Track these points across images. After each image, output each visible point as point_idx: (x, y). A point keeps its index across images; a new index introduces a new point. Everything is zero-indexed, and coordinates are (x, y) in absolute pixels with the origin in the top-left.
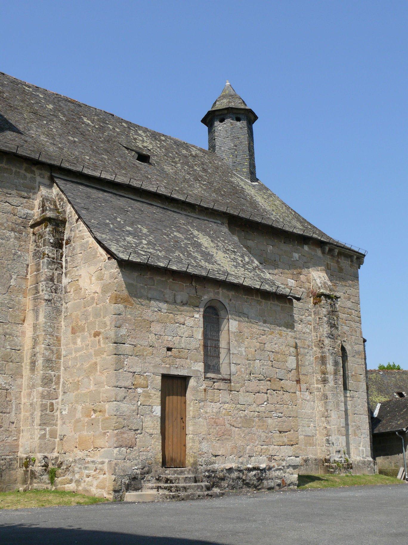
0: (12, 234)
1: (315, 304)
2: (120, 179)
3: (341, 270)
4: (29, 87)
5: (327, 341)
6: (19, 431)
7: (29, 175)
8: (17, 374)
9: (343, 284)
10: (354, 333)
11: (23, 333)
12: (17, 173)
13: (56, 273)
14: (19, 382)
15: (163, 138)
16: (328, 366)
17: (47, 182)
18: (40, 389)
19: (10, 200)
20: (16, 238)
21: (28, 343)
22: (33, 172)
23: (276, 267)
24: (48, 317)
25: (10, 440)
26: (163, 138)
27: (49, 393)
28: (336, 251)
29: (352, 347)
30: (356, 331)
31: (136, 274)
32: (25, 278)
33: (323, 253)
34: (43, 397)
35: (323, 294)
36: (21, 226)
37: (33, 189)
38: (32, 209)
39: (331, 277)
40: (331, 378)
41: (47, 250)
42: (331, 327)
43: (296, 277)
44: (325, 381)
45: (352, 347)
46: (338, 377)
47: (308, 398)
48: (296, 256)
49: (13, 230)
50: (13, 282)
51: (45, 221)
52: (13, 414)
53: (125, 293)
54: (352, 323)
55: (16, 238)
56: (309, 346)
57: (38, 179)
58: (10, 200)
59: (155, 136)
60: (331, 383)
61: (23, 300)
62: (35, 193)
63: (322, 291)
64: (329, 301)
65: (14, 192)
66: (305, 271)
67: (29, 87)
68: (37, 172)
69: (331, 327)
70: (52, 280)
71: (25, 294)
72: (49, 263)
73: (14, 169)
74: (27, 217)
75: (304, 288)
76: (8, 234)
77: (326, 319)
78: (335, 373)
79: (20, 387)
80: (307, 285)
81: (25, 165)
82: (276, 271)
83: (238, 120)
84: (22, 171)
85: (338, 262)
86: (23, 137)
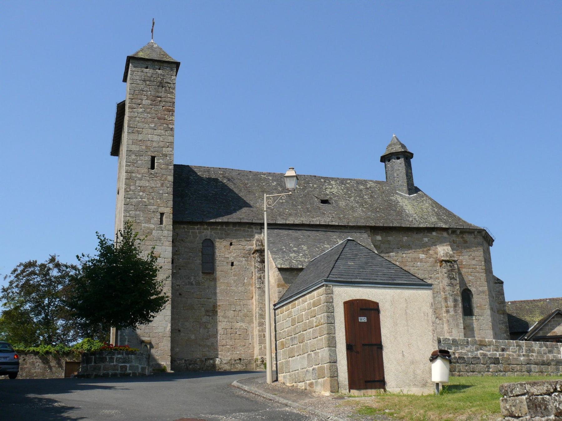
0: (244, 259)
1: (440, 266)
2: (297, 222)
3: (466, 242)
4: (264, 174)
5: (447, 288)
6: (254, 348)
7: (250, 230)
8: (251, 322)
9: (468, 250)
10: (479, 280)
11: (253, 303)
12: (244, 231)
13: (262, 275)
14: (252, 325)
15: (349, 181)
16: (449, 303)
17: (259, 231)
18: (258, 328)
19: (241, 243)
20: (245, 260)
21: (254, 309)
22: (252, 228)
23: (411, 249)
24: (259, 295)
25: (250, 351)
26: (349, 181)
27: (262, 329)
28: (458, 232)
29: (477, 289)
30: (480, 279)
31: (288, 273)
32: (252, 278)
33: (448, 234)
34: (259, 331)
35: (443, 261)
36: (247, 255)
37: (252, 236)
38: (253, 245)
39: (453, 249)
40: (451, 310)
41: (257, 265)
42: (451, 279)
43: (426, 253)
44: (448, 312)
45: (477, 289)
46: (457, 308)
47: (438, 322)
48: (426, 240)
49: (244, 257)
50: (245, 281)
51: (256, 251)
52: (250, 340)
53: (283, 282)
54: (477, 274)
55: (245, 260)
56: (437, 292)
57: (255, 231)
58: (241, 243)
59: (343, 181)
60: (452, 313)
61: (251, 288)
62: (253, 238)
63: (443, 258)
64: (449, 264)
65: (243, 239)
66: (433, 248)
67: (264, 174)
68: (254, 227)
69: (451, 279)
70: (260, 278)
71: (252, 285)
72: (258, 271)
73: (242, 229)
74: (250, 250)
75: (433, 258)
76: (241, 259)
77: (446, 275)
78: (455, 306)
79: (253, 328)
80: (435, 256)
81: (247, 226)
82: (410, 251)
83: (398, 158)
84: (246, 229)
85: (462, 238)
86: (251, 209)
